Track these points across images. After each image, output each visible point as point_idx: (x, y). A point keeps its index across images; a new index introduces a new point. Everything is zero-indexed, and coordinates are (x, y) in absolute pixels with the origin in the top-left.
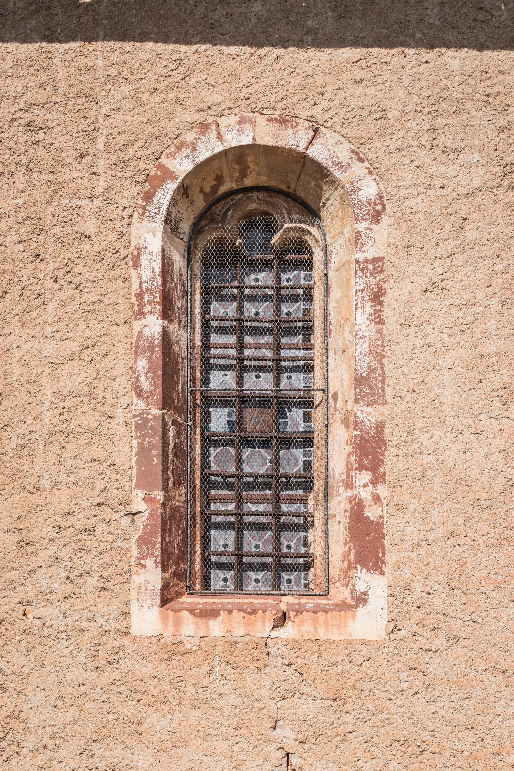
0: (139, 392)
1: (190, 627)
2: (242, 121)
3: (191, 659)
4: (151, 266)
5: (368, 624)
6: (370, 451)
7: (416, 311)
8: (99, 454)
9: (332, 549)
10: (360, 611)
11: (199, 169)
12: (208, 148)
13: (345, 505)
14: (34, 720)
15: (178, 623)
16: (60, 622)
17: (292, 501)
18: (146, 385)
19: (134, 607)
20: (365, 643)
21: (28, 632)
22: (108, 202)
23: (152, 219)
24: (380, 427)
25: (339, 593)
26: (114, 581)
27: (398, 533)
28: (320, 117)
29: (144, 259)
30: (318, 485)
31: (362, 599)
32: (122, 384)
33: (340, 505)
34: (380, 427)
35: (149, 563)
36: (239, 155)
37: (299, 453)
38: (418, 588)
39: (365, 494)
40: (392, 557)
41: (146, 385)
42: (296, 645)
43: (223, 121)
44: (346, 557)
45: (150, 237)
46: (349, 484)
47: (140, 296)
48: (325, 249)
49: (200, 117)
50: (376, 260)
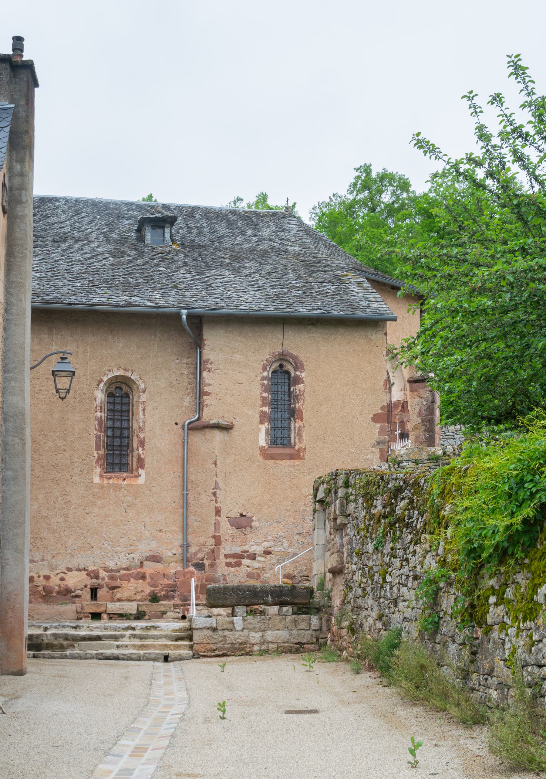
0: (96, 429)
1: (106, 481)
2: (118, 369)
3: (106, 489)
4: (98, 401)
5: (141, 481)
6: (142, 443)
7: (152, 413)
8: (88, 443)
9: (134, 463)
10: (140, 478)
11: (109, 379)
12: (111, 375)
13: (136, 454)
14: (73, 502)
15: (103, 480)
16: (79, 480)
17: (124, 451)
18: (97, 428)
19: (94, 477)
20: (140, 485)
21: (72, 482)
22: (90, 386)
23: (99, 390)
24: (144, 438)
25: (135, 473)
26: (90, 472)
27: (148, 461)
28: (133, 369)
29: (97, 399)
30: (130, 448)
31: (140, 475)
32: (92, 427)
33: (135, 453)
34: (144, 438)
35: (97, 467)
36: (116, 377)
37: (126, 440)
38: (151, 473)
39: (141, 453)
40: (146, 466)
41: (97, 428)
42: (126, 485)
43: (114, 369)
44: (137, 466)
45: (100, 395)
46: (138, 450)
47: (96, 407)
48: (133, 396)
49: (109, 368)
50: (144, 401)
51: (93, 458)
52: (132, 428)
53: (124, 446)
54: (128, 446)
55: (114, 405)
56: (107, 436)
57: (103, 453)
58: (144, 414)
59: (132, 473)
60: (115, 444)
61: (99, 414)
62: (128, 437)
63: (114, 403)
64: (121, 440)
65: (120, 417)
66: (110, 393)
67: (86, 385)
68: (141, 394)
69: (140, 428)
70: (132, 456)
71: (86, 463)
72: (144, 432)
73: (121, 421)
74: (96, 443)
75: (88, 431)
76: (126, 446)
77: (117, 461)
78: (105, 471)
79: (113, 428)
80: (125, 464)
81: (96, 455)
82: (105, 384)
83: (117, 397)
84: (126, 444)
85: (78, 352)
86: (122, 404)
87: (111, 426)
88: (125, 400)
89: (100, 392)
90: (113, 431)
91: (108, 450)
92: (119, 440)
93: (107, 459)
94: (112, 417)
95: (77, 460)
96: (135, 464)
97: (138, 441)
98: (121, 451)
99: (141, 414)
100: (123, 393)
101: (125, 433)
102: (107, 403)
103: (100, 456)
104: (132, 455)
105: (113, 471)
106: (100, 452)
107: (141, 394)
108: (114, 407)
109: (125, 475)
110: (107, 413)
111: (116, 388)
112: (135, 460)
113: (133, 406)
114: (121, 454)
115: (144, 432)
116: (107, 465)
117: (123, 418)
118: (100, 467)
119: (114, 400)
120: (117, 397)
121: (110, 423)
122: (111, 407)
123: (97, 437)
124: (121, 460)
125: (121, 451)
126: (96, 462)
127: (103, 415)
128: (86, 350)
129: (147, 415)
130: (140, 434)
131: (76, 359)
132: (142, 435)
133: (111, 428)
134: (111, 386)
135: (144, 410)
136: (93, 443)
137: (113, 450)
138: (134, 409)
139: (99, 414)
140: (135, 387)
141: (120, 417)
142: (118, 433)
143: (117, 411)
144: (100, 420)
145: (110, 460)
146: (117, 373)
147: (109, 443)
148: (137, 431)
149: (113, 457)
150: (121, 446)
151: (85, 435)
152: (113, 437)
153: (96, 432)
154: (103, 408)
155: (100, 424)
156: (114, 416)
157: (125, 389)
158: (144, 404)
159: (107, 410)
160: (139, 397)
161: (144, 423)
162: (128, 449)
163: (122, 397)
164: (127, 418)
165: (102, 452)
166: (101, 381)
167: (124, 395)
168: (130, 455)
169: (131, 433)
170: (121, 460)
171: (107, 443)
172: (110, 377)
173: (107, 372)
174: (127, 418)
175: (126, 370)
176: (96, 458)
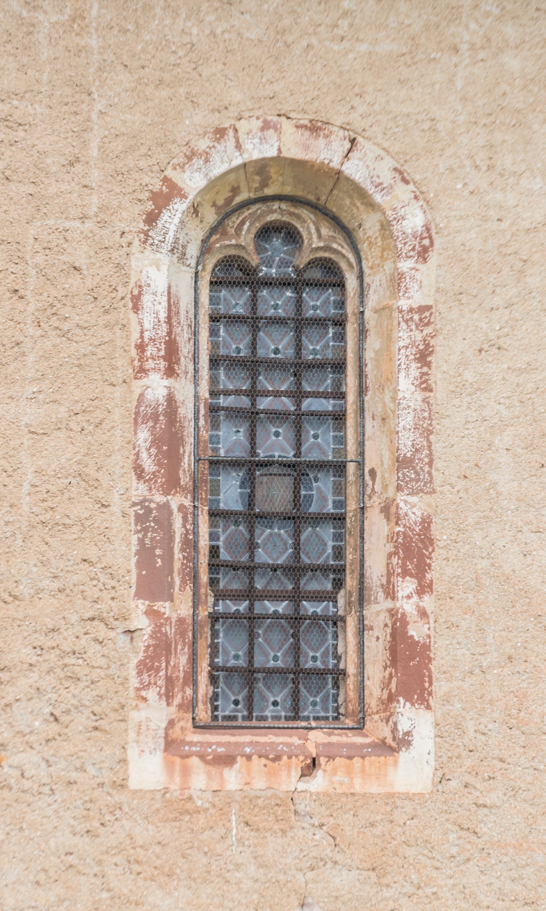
0: (139, 472)
1: (200, 779)
2: (266, 126)
3: (202, 820)
4: (154, 307)
5: (412, 772)
6: (415, 552)
7: (469, 376)
8: (92, 553)
9: (369, 670)
10: (403, 756)
11: (213, 185)
12: (225, 160)
13: (384, 618)
15: (186, 772)
16: (42, 772)
18: (149, 465)
19: (132, 753)
20: (409, 797)
22: (103, 224)
24: (426, 523)
25: (377, 729)
27: (447, 658)
28: (358, 124)
29: (146, 300)
30: (351, 582)
31: (404, 742)
32: (120, 463)
33: (377, 612)
34: (426, 523)
35: (151, 694)
37: (327, 533)
38: (470, 726)
39: (409, 607)
40: (440, 687)
41: (149, 465)
42: (325, 799)
44: (386, 685)
45: (166, 278)
46: (390, 593)
47: (141, 347)
48: (361, 277)
49: (215, 120)
50: (422, 309)
51: (123, 640)
52: (360, 465)
53: (314, 569)
54: (342, 570)
55: (255, 330)
56: (214, 514)
57: (184, 609)
58: (425, 385)
59: (360, 727)
60: (262, 556)
61: (156, 386)
62: (339, 519)
63: (253, 322)
64: (297, 536)
65: (287, 404)
66: (228, 263)
67: (83, 218)
68: (405, 265)
69: (402, 463)
70: (361, 630)
71: (81, 672)
72: (425, 486)
73: (297, 421)
74: (145, 554)
75: (96, 484)
76: (325, 569)
77: (273, 654)
78: (204, 714)
79: (252, 467)
80: (321, 673)
81: (141, 622)
82: (195, 210)
83: (268, 283)
84: (327, 556)
85: (31, 28)
86: (300, 324)
87: (240, 454)
88: (316, 303)
89: (165, 258)
90: (249, 482)
91: (220, 596)
92: (282, 532)
93: (214, 648)
94: (244, 402)
95: (28, 654)
96: (376, 674)
97: (391, 538)
98: (296, 597)
99: (406, 384)
100: (302, 260)
101: (321, 492)
102: (214, 319)
103: (170, 630)
104: (361, 619)
105: (250, 714)
106: (164, 607)
107: (405, 265)
108: (253, 345)
109: (317, 737)
110: (214, 380)
111: (266, 233)
112: (377, 649)
113: (362, 332)
114: (296, 619)
115: (425, 486)
116: (213, 680)
117: (308, 404)
118: (168, 697)
119: (254, 301)
120: (268, 283)
121: (232, 439)
122: (236, 344)
123: (148, 518)
124: (296, 651)
125: (296, 597)
126: (146, 667)
127: (184, 390)
128: (78, 17)
129: (440, 393)
130: (401, 498)
131: (22, 69)
132: (412, 507)
133: (235, 464)
134: (235, 220)
135: (424, 357)
136: (123, 551)
137: (250, 594)
138: (369, 355)
139: (156, 386)
140: (369, 226)
141: (288, 404)
142: (276, 493)
143: (273, 365)
144: (166, 423)
145: (233, 653)
146: (258, 150)
147: (224, 555)
148: (384, 484)
149: (252, 637)
150: (295, 570)
151: (79, 510)
152: (252, 517)
153: (139, 490)
154: (185, 350)
155: (168, 441)
156: (253, 393)
157: (316, 236)
158: (424, 323)
159: (214, 362)
160: (397, 282)
161: (428, 433)
162: (339, 584)
163: (298, 284)
164: (329, 405)
165: (179, 606)
166: (163, 198)
167: (316, 274)
168: (351, 623)
169: (352, 491)
170: (296, 651)
171: (214, 551)
172: (219, 168)
173: (203, 144)
174: (329, 405)
175: (314, 128)
176: (144, 640)
